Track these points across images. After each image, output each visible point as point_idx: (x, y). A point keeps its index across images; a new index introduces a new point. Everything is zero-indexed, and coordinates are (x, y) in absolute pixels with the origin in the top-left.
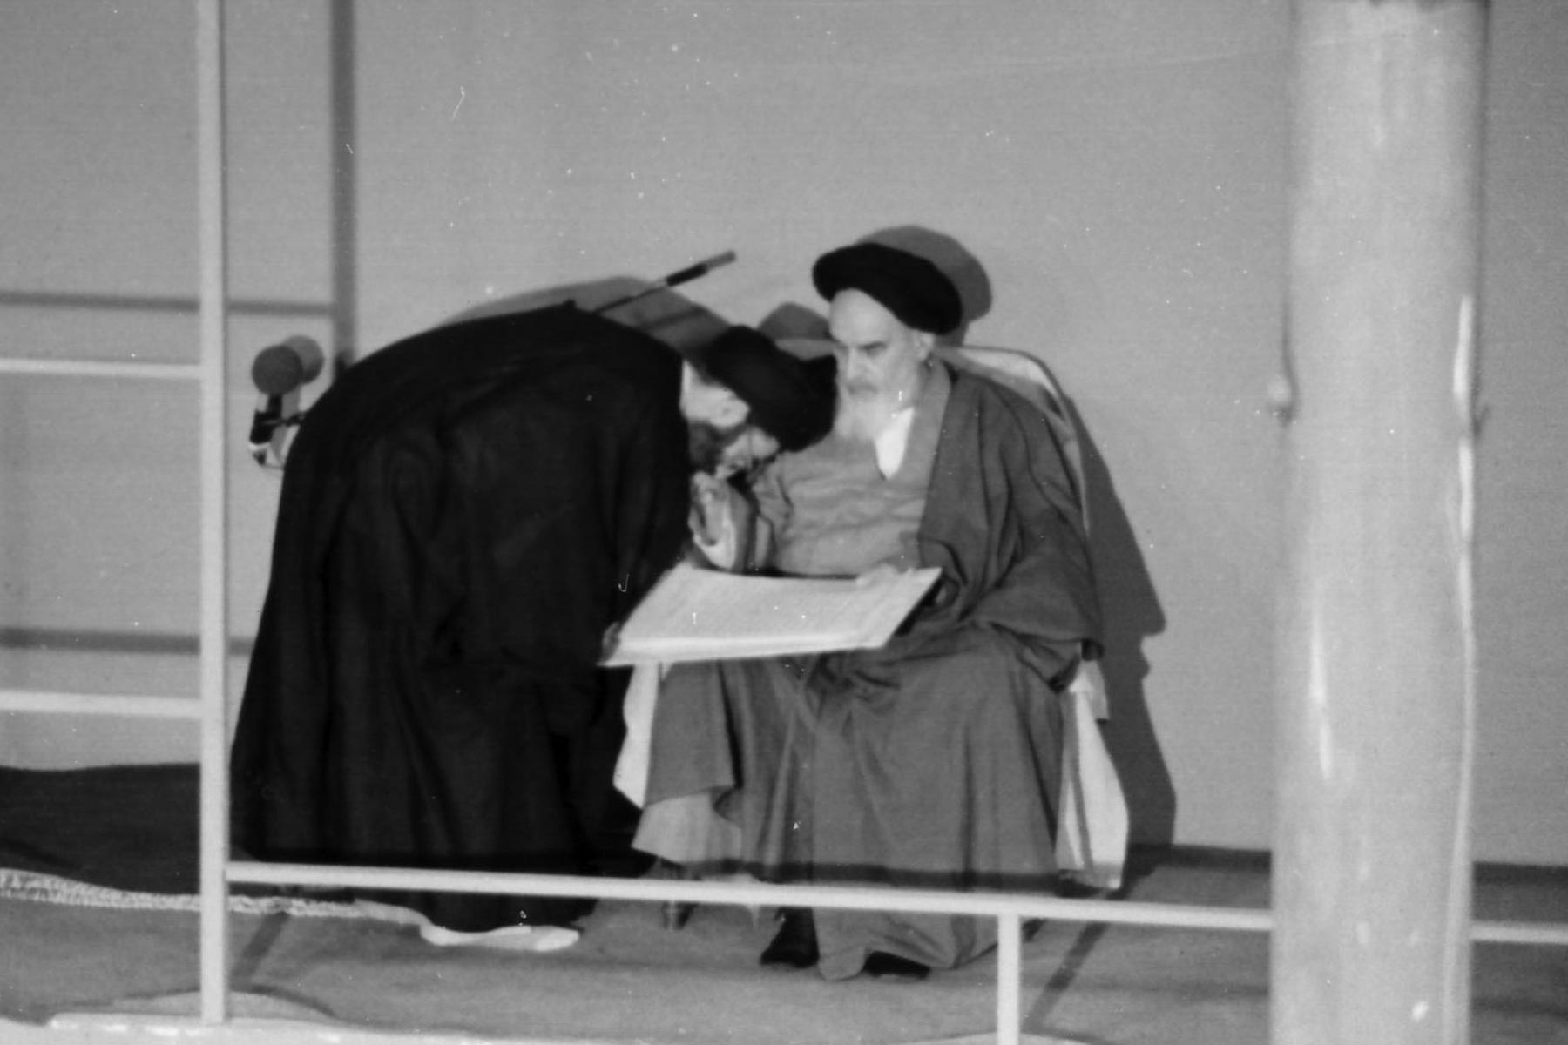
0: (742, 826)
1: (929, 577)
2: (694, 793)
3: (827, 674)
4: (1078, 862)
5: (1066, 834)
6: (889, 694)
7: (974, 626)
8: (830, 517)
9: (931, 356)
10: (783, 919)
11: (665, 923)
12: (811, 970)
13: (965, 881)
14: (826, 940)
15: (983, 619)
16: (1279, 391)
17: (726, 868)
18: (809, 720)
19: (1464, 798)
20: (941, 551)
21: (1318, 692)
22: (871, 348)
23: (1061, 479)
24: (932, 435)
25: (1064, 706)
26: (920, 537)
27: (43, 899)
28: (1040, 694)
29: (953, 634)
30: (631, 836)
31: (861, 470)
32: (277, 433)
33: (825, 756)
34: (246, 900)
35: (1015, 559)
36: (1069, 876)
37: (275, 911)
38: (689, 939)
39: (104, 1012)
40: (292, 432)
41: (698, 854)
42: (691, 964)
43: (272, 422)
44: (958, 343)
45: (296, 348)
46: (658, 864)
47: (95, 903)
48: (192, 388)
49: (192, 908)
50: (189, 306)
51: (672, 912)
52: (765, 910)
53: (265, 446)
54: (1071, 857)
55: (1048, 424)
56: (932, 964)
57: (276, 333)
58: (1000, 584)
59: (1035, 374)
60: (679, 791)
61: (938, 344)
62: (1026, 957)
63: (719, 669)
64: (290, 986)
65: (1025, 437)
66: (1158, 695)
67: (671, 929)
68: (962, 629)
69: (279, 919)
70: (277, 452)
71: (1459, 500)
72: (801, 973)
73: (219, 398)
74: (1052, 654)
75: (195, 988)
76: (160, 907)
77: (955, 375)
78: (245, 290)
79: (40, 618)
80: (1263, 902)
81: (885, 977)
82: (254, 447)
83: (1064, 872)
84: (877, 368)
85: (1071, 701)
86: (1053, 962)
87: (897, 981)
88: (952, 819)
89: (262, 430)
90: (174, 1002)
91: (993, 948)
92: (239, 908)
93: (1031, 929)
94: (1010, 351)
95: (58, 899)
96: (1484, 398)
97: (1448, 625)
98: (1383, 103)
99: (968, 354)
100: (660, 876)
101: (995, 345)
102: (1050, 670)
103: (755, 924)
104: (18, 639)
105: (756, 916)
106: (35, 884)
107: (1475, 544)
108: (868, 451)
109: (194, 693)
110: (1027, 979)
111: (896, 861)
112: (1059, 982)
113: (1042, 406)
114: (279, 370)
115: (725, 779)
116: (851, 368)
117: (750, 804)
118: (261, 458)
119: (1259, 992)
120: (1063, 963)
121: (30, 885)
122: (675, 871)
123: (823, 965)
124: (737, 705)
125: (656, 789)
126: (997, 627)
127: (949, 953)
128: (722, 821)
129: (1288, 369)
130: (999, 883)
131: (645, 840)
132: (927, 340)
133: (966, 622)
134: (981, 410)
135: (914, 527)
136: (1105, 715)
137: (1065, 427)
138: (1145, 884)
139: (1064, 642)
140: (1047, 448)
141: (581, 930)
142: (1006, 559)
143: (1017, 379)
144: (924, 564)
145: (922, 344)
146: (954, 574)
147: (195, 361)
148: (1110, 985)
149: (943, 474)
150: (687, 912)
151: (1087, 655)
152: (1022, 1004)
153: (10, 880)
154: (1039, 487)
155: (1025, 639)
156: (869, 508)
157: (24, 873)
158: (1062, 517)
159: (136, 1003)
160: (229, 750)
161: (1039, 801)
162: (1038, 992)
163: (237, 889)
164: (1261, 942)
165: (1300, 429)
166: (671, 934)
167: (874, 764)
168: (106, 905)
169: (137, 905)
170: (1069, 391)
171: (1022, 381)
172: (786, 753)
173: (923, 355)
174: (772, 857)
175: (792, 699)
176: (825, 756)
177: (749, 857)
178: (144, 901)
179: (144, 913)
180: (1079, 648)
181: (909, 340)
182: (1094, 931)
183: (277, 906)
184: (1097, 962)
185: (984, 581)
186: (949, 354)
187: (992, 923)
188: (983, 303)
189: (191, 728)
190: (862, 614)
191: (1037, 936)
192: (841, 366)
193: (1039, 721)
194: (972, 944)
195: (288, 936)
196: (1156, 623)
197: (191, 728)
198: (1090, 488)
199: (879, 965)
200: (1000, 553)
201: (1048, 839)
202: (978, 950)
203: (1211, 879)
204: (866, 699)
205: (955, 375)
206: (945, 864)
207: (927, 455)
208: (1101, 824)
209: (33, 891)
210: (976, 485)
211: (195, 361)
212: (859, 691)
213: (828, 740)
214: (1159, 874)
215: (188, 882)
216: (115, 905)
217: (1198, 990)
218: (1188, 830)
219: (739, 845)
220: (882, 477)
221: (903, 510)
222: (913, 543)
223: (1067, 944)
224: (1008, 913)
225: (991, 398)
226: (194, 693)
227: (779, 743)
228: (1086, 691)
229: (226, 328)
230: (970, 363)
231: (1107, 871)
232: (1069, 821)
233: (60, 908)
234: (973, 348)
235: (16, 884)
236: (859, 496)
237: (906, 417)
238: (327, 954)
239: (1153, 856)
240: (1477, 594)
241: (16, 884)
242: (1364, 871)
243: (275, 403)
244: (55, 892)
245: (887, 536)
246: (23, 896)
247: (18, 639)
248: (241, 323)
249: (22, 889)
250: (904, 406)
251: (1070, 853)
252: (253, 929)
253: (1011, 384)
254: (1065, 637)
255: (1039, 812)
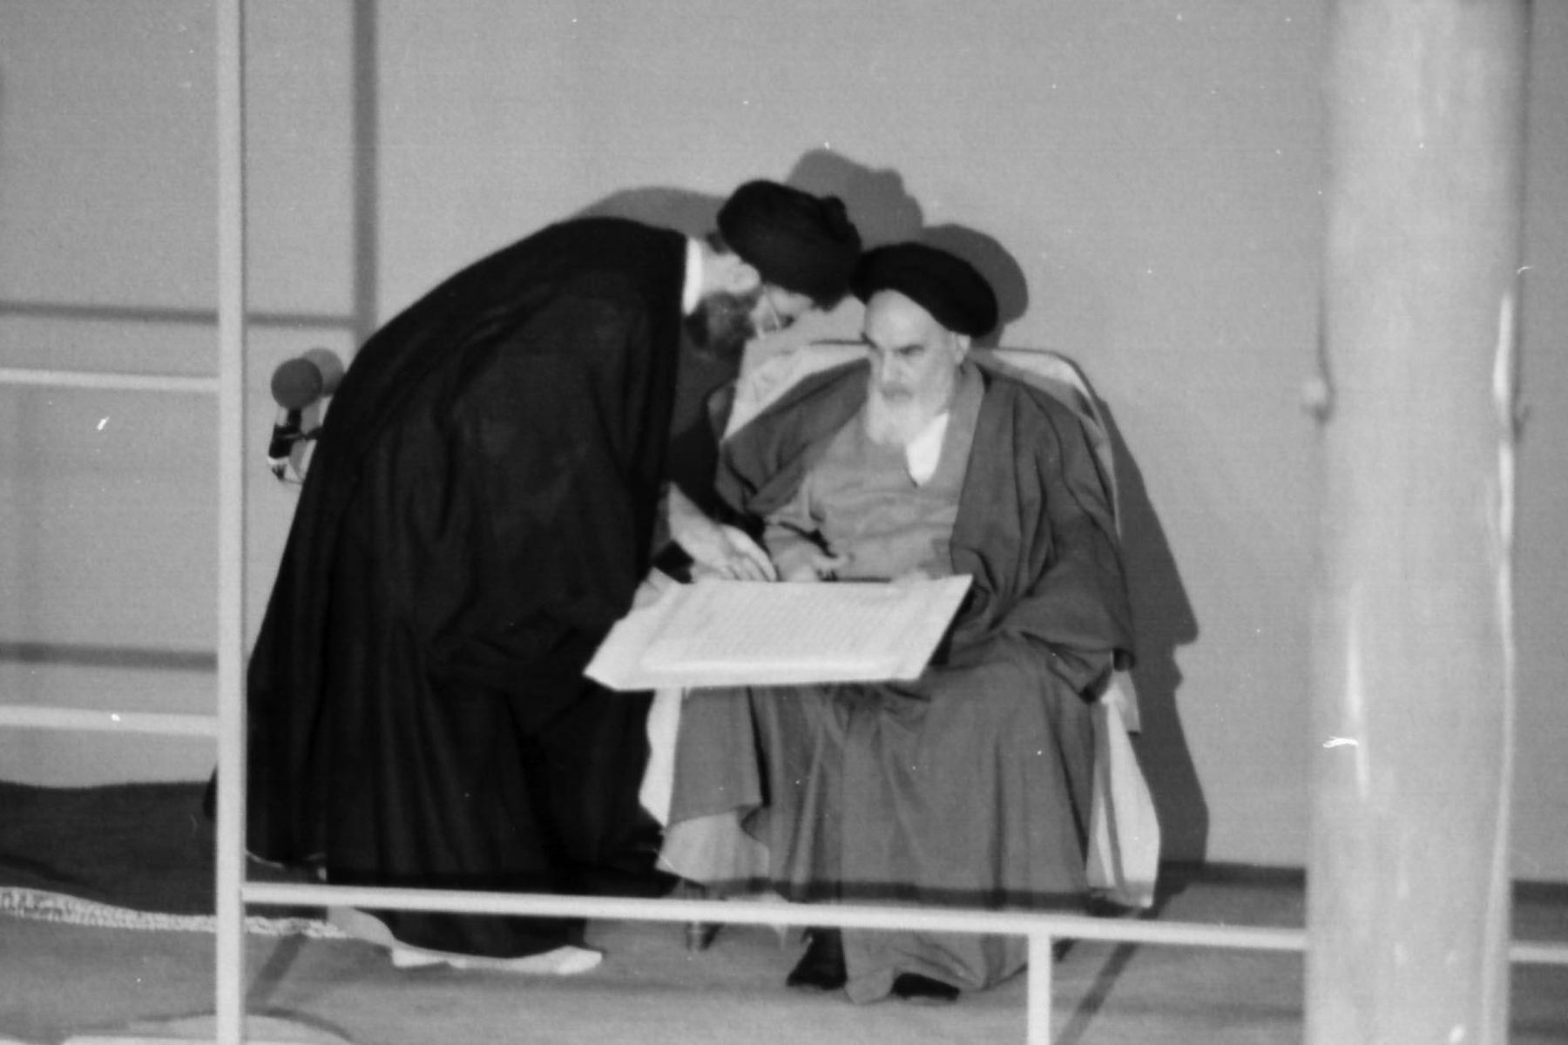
0: (770, 846)
1: (959, 586)
2: (720, 810)
3: (854, 698)
4: (1110, 879)
5: (1098, 854)
6: (919, 707)
7: (1004, 635)
8: (860, 526)
9: (966, 359)
10: (810, 940)
11: (689, 942)
12: (839, 992)
13: (996, 899)
14: (855, 962)
15: (1013, 627)
16: (1314, 391)
17: (754, 887)
18: (838, 735)
19: (1503, 813)
20: (974, 558)
21: (1355, 701)
22: (907, 351)
23: (1095, 485)
24: (966, 438)
25: (1095, 718)
26: (952, 544)
27: (57, 918)
28: (1071, 703)
29: (984, 643)
30: (654, 857)
31: (891, 479)
32: (296, 448)
33: (856, 766)
34: (263, 921)
35: (1047, 566)
36: (1099, 895)
37: (291, 933)
38: (715, 961)
39: (119, 1035)
40: (310, 447)
41: (726, 874)
42: (716, 987)
43: (290, 436)
44: (994, 344)
45: (317, 361)
46: (681, 886)
47: (111, 923)
48: (209, 402)
49: (211, 930)
50: (209, 318)
51: (697, 933)
52: (792, 930)
53: (285, 461)
54: (1102, 874)
55: (1080, 422)
56: (960, 985)
57: (296, 344)
58: (1030, 592)
59: (1068, 375)
60: (702, 810)
61: (974, 345)
62: (1056, 977)
63: (750, 693)
64: (306, 1008)
65: (1059, 440)
66: (1192, 706)
67: (695, 951)
68: (992, 639)
69: (295, 942)
70: (297, 469)
71: (1498, 503)
72: (829, 995)
73: (233, 406)
74: (1085, 664)
75: (211, 1011)
76: (178, 928)
77: (988, 378)
78: (263, 303)
79: (51, 634)
80: (1297, 921)
81: (914, 999)
82: (273, 462)
83: (1095, 890)
84: (911, 371)
85: (1103, 711)
86: (1084, 984)
87: (926, 1004)
88: (983, 839)
89: (281, 445)
90: (191, 1025)
91: (1023, 969)
92: (256, 930)
93: (1062, 949)
94: (1041, 352)
95: (74, 919)
96: (1524, 400)
97: (1487, 634)
98: (1418, 84)
99: (1000, 356)
100: (684, 897)
101: (1030, 348)
102: (1082, 679)
103: (783, 943)
104: (32, 653)
105: (783, 935)
106: (49, 903)
107: (1517, 552)
108: (898, 459)
109: (210, 711)
110: (1058, 1002)
111: (927, 878)
112: (1091, 1004)
113: (1072, 404)
114: (294, 383)
115: (753, 798)
116: (887, 370)
117: (778, 822)
118: (280, 473)
119: (1295, 1014)
120: (1095, 980)
121: (42, 905)
122: (699, 890)
123: (852, 988)
124: (770, 732)
125: (681, 806)
126: (1028, 636)
127: (979, 974)
128: (749, 840)
129: (1324, 369)
130: (1029, 901)
131: (667, 862)
132: (964, 341)
133: (996, 632)
134: (1016, 414)
135: (946, 534)
136: (1137, 727)
137: (1097, 430)
138: (1176, 902)
139: (1092, 652)
140: (1081, 452)
141: (604, 952)
142: (1038, 566)
143: (1047, 379)
144: (956, 570)
145: (959, 347)
146: (985, 582)
147: (214, 375)
148: (1139, 1007)
149: (976, 477)
150: (712, 933)
151: (1118, 665)
152: (1053, 1029)
153: (23, 898)
154: (1072, 493)
155: (1058, 648)
156: (902, 514)
157: (39, 892)
158: (1093, 522)
159: (152, 1027)
160: (246, 665)
161: (1070, 817)
162: (1065, 1019)
163: (253, 909)
164: (1296, 960)
165: (1333, 430)
166: (695, 956)
167: (905, 781)
168: (122, 925)
169: (152, 926)
170: (1101, 394)
171: (1059, 385)
172: (815, 769)
173: (959, 358)
174: (800, 876)
175: (824, 720)
176: (856, 766)
177: (777, 875)
178: (160, 921)
179: (160, 934)
180: (1111, 657)
181: (946, 342)
182: (1125, 951)
183: (294, 928)
184: (1129, 983)
185: (1015, 589)
186: (983, 356)
187: (1022, 942)
188: (1020, 304)
189: (211, 744)
190: (888, 630)
191: (1068, 956)
192: (875, 370)
193: (1070, 731)
194: (1002, 966)
195: (305, 958)
196: (1188, 631)
197: (211, 744)
198: (1121, 487)
199: (908, 987)
200: (1031, 562)
201: (1080, 859)
202: (1007, 972)
203: (1246, 898)
204: (891, 711)
205: (988, 378)
206: (974, 878)
207: (960, 459)
208: (1133, 841)
209: (47, 910)
210: (1010, 491)
211: (214, 375)
212: (888, 704)
213: (856, 755)
214: (1193, 894)
215: (205, 903)
216: (130, 926)
217: (1231, 1012)
218: (1221, 846)
219: (767, 863)
220: (915, 484)
221: (937, 517)
222: (945, 549)
223: (1099, 963)
224: (1038, 931)
225: (1024, 396)
226: (210, 711)
227: (807, 762)
228: (1118, 701)
229: (244, 342)
230: (1001, 364)
231: (1140, 888)
232: (1100, 838)
233: (72, 928)
234: (1005, 349)
235: (30, 903)
236: (890, 502)
237: (942, 421)
238: (342, 976)
239: (1186, 874)
240: (1517, 604)
241: (30, 903)
242: (1403, 889)
243: (295, 417)
244: (69, 912)
245: (921, 542)
246: (37, 916)
247: (32, 653)
248: (258, 335)
249: (36, 908)
250: (940, 412)
251: (1102, 871)
252: (269, 952)
253: (1046, 388)
254: (1096, 646)
255: (1070, 829)
